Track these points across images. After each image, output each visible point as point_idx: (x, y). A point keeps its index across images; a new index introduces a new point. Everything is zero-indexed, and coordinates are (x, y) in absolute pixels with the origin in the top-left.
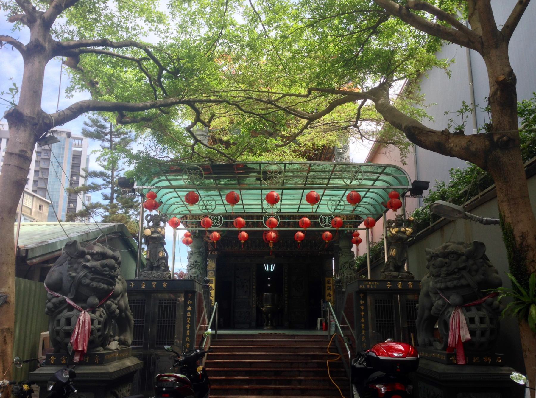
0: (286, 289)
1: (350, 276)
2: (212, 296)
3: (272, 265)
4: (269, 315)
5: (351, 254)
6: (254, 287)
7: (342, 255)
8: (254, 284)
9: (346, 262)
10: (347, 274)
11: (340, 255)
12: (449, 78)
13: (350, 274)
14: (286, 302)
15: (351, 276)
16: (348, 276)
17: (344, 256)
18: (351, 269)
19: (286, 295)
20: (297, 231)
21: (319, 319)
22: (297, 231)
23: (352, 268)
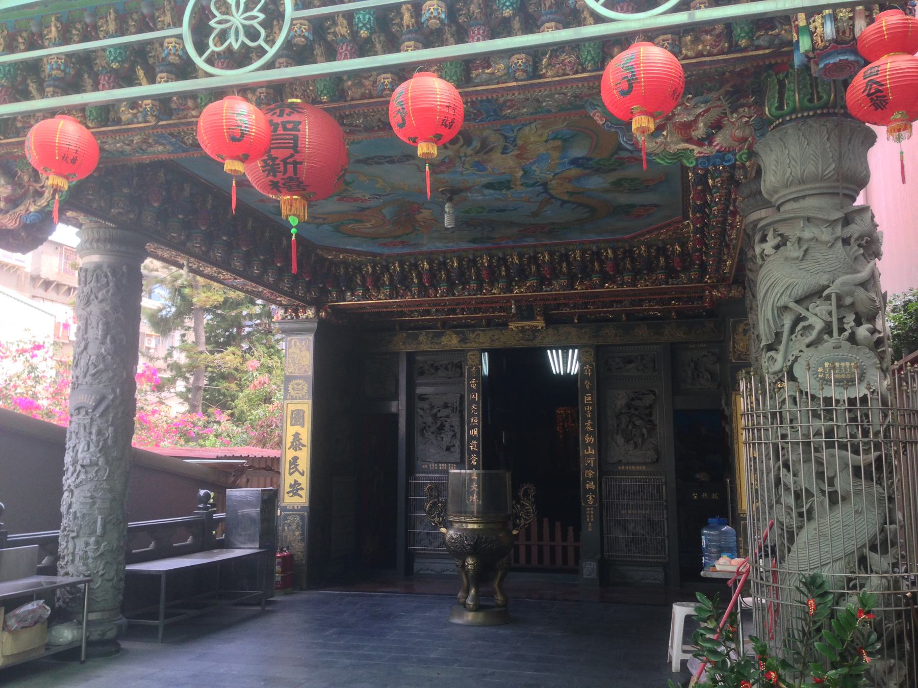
0: (589, 439)
1: (845, 395)
2: (300, 468)
3: (571, 351)
4: (470, 561)
5: (854, 230)
6: (475, 432)
7: (783, 241)
8: (475, 421)
9: (817, 293)
10: (826, 382)
11: (768, 247)
12: (834, 348)
13: (848, 383)
14: (591, 485)
15: (859, 391)
16: (832, 392)
17: (792, 251)
18: (852, 339)
19: (591, 461)
20: (403, 73)
21: (680, 612)
22: (403, 73)
23: (863, 331)
